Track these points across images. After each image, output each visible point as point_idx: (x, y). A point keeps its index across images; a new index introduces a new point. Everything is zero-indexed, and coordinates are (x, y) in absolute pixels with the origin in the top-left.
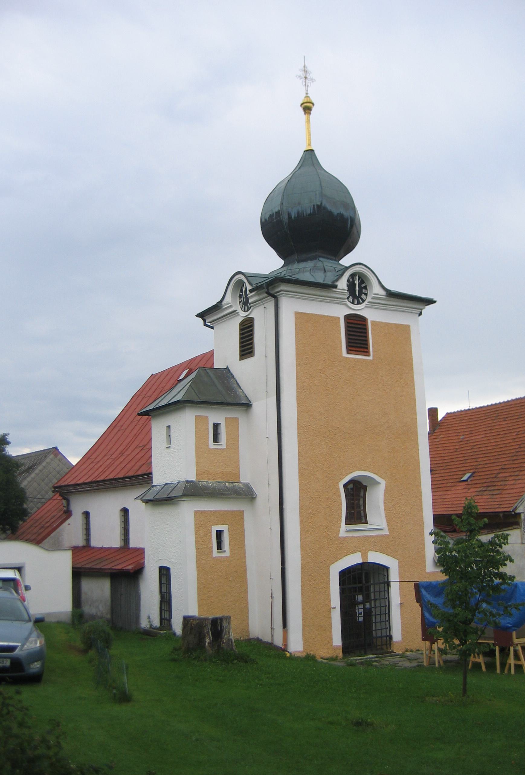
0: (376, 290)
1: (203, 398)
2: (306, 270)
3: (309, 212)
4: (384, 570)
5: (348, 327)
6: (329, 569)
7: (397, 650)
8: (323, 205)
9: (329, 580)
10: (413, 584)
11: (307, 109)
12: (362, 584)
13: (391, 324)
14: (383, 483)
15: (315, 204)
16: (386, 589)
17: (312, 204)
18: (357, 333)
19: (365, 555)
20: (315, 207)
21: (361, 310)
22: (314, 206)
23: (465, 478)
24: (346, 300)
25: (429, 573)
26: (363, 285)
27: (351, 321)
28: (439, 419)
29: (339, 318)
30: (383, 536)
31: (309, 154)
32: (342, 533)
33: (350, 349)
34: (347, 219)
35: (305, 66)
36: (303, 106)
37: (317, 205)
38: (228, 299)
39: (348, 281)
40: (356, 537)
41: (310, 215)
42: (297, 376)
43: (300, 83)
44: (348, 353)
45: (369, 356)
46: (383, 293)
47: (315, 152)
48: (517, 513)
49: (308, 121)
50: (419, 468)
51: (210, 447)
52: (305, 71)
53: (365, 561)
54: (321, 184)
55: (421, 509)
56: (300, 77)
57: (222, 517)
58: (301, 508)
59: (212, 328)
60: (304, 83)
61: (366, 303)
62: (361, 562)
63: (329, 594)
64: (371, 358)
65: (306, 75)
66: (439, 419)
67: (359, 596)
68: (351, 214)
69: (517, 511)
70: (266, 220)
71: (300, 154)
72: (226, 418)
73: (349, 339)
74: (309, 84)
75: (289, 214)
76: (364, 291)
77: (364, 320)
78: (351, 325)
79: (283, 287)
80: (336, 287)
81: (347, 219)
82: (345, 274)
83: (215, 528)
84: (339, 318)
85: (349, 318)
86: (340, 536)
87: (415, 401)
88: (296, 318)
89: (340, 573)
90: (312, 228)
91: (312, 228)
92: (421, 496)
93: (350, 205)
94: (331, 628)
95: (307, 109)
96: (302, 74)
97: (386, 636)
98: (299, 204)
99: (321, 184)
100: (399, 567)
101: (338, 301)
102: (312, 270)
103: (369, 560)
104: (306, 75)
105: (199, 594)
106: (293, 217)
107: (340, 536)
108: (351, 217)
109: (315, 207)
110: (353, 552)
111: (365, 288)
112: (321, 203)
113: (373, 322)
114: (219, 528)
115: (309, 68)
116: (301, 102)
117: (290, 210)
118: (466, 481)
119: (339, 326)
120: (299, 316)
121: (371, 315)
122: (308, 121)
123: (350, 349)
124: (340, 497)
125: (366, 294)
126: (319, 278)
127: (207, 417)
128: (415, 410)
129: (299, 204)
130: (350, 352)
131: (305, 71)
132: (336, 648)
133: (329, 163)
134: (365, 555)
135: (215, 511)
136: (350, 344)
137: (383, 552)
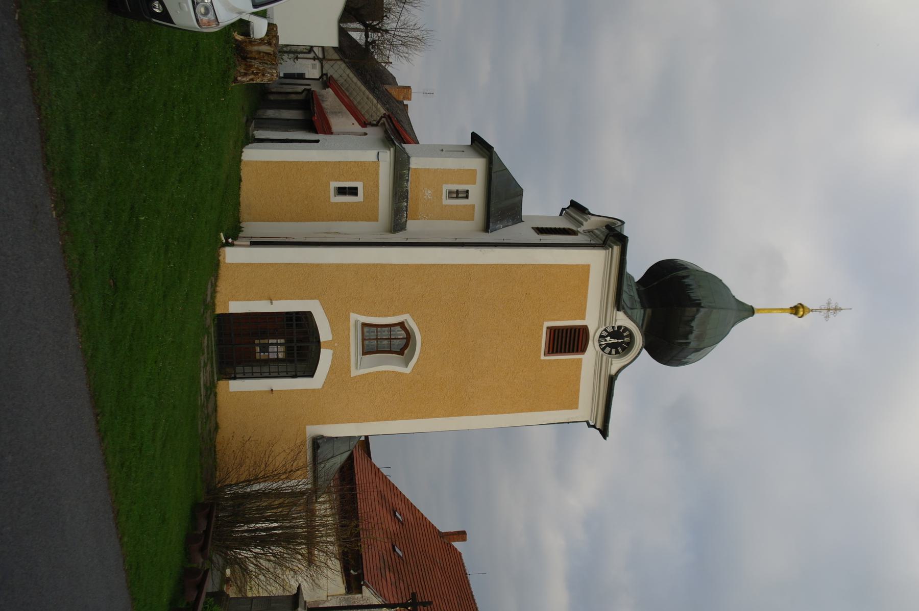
0: (617, 364)
1: (494, 175)
2: (631, 293)
3: (692, 295)
4: (310, 373)
6: (315, 298)
7: (222, 384)
11: (796, 310)
12: (293, 342)
14: (407, 370)
16: (289, 374)
18: (568, 340)
19: (329, 345)
21: (593, 348)
23: (397, 549)
25: (305, 428)
26: (619, 349)
29: (584, 319)
30: (349, 370)
32: (354, 317)
39: (626, 329)
40: (349, 335)
43: (823, 304)
45: (550, 329)
46: (613, 372)
47: (751, 318)
48: (361, 589)
52: (836, 309)
53: (322, 345)
56: (829, 303)
57: (373, 194)
59: (561, 214)
63: (287, 299)
65: (831, 309)
68: (693, 344)
69: (364, 587)
71: (748, 302)
72: (473, 206)
76: (614, 351)
77: (582, 349)
79: (617, 249)
83: (359, 185)
84: (584, 319)
85: (584, 330)
89: (310, 313)
90: (674, 310)
91: (674, 310)
92: (392, 419)
93: (701, 349)
95: (796, 310)
96: (833, 306)
97: (235, 373)
98: (700, 286)
100: (314, 390)
103: (322, 350)
104: (831, 309)
110: (332, 330)
111: (617, 352)
114: (360, 191)
115: (839, 313)
120: (586, 269)
124: (394, 315)
125: (610, 353)
126: (625, 296)
127: (474, 183)
131: (836, 309)
134: (329, 345)
135: (378, 186)
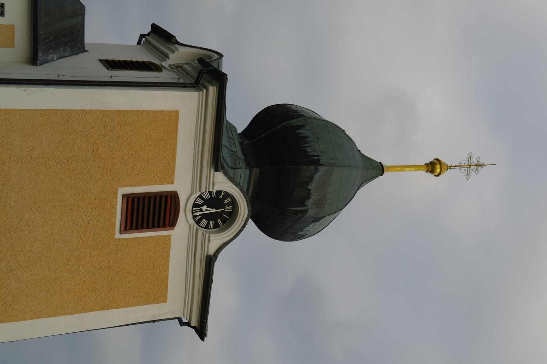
0: (216, 240)
2: (231, 149)
3: (309, 150)
5: (161, 197)
8: (320, 168)
11: (433, 167)
13: (167, 270)
15: (320, 158)
17: (320, 154)
18: (151, 212)
20: (316, 158)
21: (185, 221)
22: (318, 156)
24: (198, 194)
26: (219, 221)
27: (169, 201)
29: (172, 183)
31: (379, 169)
33: (130, 199)
35: (483, 165)
36: (435, 161)
37: (319, 160)
38: (182, 49)
41: (305, 151)
42: (88, 111)
43: (463, 159)
44: (124, 196)
45: (121, 232)
46: (212, 252)
54: (345, 166)
56: (470, 158)
59: (139, 43)
60: (463, 163)
61: (196, 226)
64: (118, 236)
65: (473, 166)
70: (290, 107)
71: (377, 158)
73: (144, 198)
74: (462, 171)
75: (302, 127)
76: (212, 223)
78: (163, 200)
79: (212, 90)
82: (234, 187)
84: (172, 183)
87: (54, 316)
88: (170, 112)
95: (433, 167)
96: (474, 161)
98: (318, 139)
99: (345, 166)
101: (198, 178)
102: (233, 153)
104: (473, 166)
106: (300, 131)
108: (307, 211)
109: (316, 158)
111: (216, 226)
112: (322, 165)
113: (168, 239)
115: (482, 170)
116: (440, 159)
117: (307, 127)
119: (162, 183)
120: (172, 117)
121: (182, 233)
123: (130, 199)
125: (207, 227)
128: (39, 318)
129: (318, 139)
130: (125, 199)
136: (136, 200)
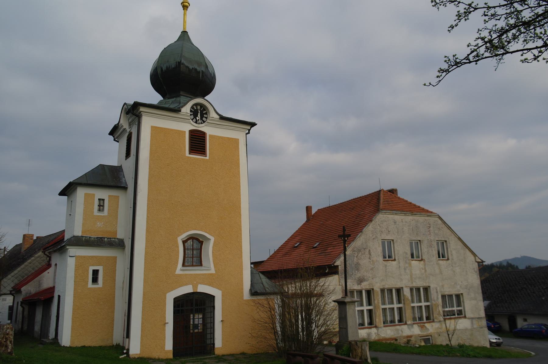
0: (213, 114)
1: (89, 182)
3: (173, 66)
4: (212, 298)
9: (165, 304)
10: (51, 285)
13: (225, 137)
14: (212, 239)
16: (212, 311)
18: (198, 143)
19: (195, 286)
21: (203, 128)
23: (315, 246)
28: (313, 213)
29: (185, 132)
30: (211, 274)
31: (184, 33)
32: (178, 272)
34: (199, 72)
38: (121, 122)
39: (192, 107)
44: (190, 154)
46: (218, 117)
49: (185, 14)
50: (241, 230)
51: (94, 214)
55: (241, 257)
57: (99, 260)
58: (146, 253)
59: (118, 142)
62: (192, 291)
63: (165, 314)
66: (313, 213)
67: (196, 316)
69: (335, 264)
75: (162, 69)
76: (205, 116)
77: (203, 134)
79: (142, 109)
80: (180, 111)
81: (199, 72)
83: (91, 268)
84: (185, 132)
85: (192, 132)
86: (176, 273)
90: (182, 78)
91: (182, 78)
93: (206, 64)
94: (165, 338)
97: (211, 344)
98: (168, 61)
101: (183, 120)
103: (198, 291)
105: (73, 313)
107: (176, 273)
110: (186, 284)
111: (206, 114)
113: (210, 136)
114: (96, 268)
118: (316, 247)
122: (185, 14)
124: (178, 247)
125: (206, 118)
132: (169, 351)
133: (196, 40)
134: (195, 286)
135: (93, 257)
137: (210, 285)
